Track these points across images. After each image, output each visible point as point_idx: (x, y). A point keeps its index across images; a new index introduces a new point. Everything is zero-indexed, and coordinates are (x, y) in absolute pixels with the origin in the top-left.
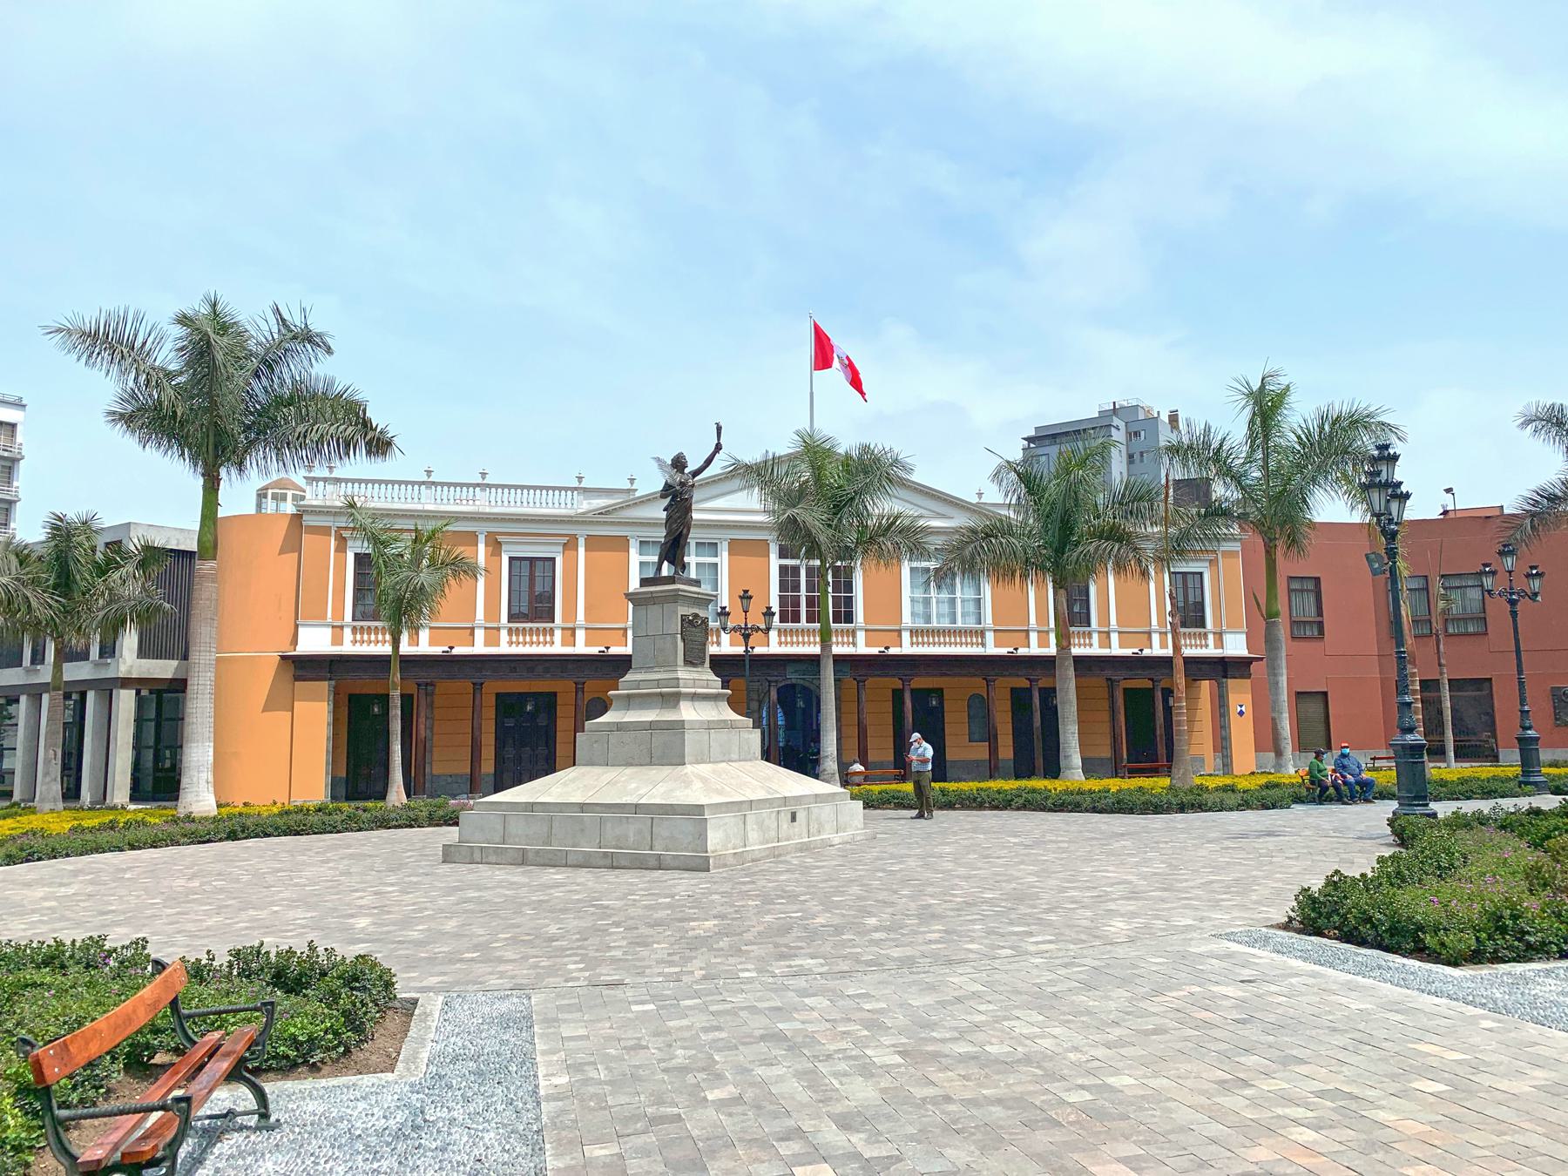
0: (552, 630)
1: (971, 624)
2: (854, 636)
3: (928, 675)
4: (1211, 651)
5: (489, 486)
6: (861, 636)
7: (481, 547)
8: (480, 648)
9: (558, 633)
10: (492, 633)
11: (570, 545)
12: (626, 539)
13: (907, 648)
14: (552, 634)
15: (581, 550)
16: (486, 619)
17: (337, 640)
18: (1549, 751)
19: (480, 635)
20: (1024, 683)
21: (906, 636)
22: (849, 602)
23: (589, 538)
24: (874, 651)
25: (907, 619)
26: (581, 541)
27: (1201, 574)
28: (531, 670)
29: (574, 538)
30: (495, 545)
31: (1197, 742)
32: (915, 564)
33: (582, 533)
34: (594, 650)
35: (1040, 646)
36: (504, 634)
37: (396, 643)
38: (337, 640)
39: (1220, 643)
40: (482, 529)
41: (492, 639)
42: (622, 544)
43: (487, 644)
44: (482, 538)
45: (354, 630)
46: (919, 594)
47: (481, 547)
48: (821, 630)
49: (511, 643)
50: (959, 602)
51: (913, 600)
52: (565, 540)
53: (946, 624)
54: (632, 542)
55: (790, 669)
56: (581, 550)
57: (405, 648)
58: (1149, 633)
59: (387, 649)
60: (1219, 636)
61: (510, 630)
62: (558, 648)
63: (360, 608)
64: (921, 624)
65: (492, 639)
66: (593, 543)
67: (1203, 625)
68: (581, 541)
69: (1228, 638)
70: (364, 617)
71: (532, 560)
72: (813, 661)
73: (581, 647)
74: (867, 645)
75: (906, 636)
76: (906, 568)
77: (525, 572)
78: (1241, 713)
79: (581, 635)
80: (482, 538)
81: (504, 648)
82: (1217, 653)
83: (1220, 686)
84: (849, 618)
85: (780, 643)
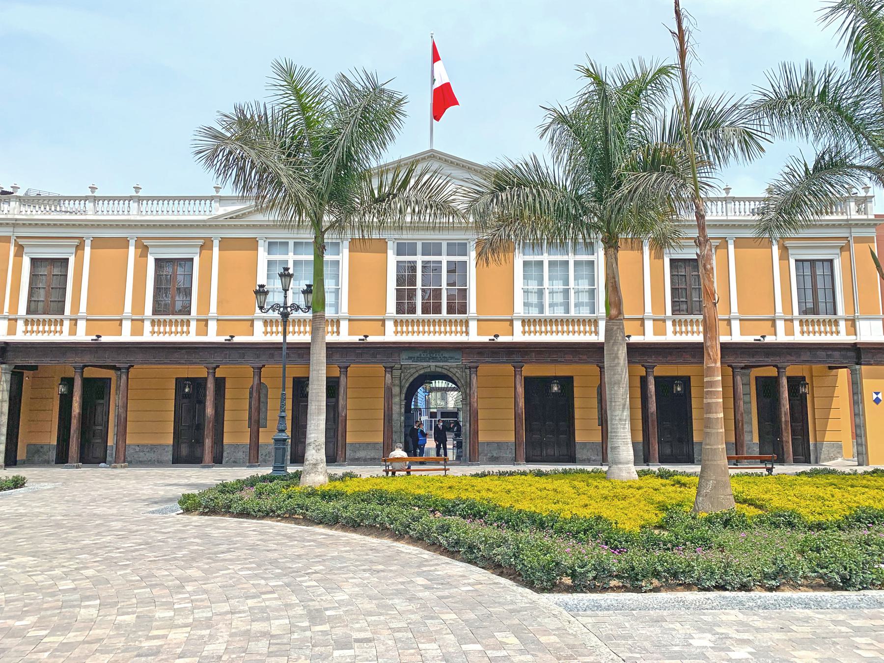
0: (188, 321)
1: (585, 313)
2: (467, 326)
3: (538, 362)
4: (843, 337)
5: (734, 199)
6: (473, 325)
7: (132, 249)
8: (126, 336)
9: (193, 324)
10: (137, 323)
11: (206, 245)
12: (384, 242)
13: (519, 336)
14: (188, 325)
15: (216, 250)
16: (133, 312)
17: (12, 331)
18: (376, 441)
19: (127, 325)
20: (772, 372)
21: (517, 325)
22: (463, 293)
23: (223, 240)
24: (485, 339)
25: (519, 309)
26: (216, 243)
27: (831, 261)
28: (480, 354)
29: (82, 240)
30: (143, 250)
31: (834, 427)
32: (579, 258)
33: (216, 235)
34: (355, 339)
35: (656, 333)
36: (147, 325)
37: (285, 334)
38: (12, 331)
39: (73, 332)
40: (132, 235)
41: (137, 330)
42: (253, 244)
43: (133, 333)
44: (132, 242)
45: (153, 322)
46: (533, 286)
47: (132, 249)
48: (705, 320)
49: (153, 333)
50: (572, 292)
51: (526, 292)
52: (201, 242)
53: (559, 313)
54: (261, 242)
55: (404, 355)
56: (216, 250)
57: (290, 339)
58: (773, 321)
59: (279, 339)
60: (852, 323)
61: (801, 321)
62: (192, 336)
63: (33, 304)
64: (534, 313)
65: (137, 330)
66: (97, 243)
67: (62, 312)
68: (216, 243)
69: (862, 325)
70: (805, 312)
71: (813, 262)
72: (695, 351)
73: (213, 336)
74: (655, 334)
75: (517, 325)
76: (519, 260)
77: (808, 272)
78: (877, 401)
79: (213, 326)
80: (132, 242)
81: (148, 336)
82: (851, 339)
83: (853, 373)
84: (463, 309)
85: (524, 333)
